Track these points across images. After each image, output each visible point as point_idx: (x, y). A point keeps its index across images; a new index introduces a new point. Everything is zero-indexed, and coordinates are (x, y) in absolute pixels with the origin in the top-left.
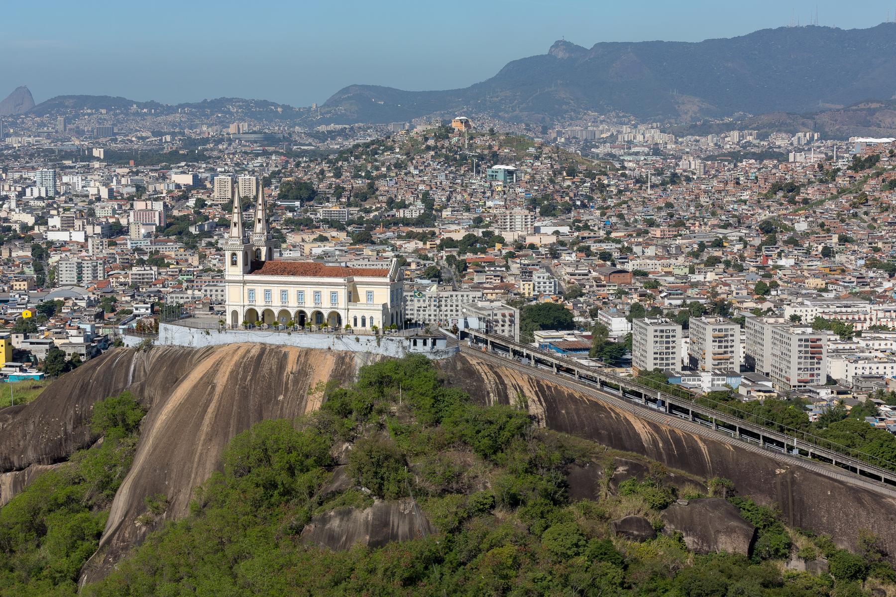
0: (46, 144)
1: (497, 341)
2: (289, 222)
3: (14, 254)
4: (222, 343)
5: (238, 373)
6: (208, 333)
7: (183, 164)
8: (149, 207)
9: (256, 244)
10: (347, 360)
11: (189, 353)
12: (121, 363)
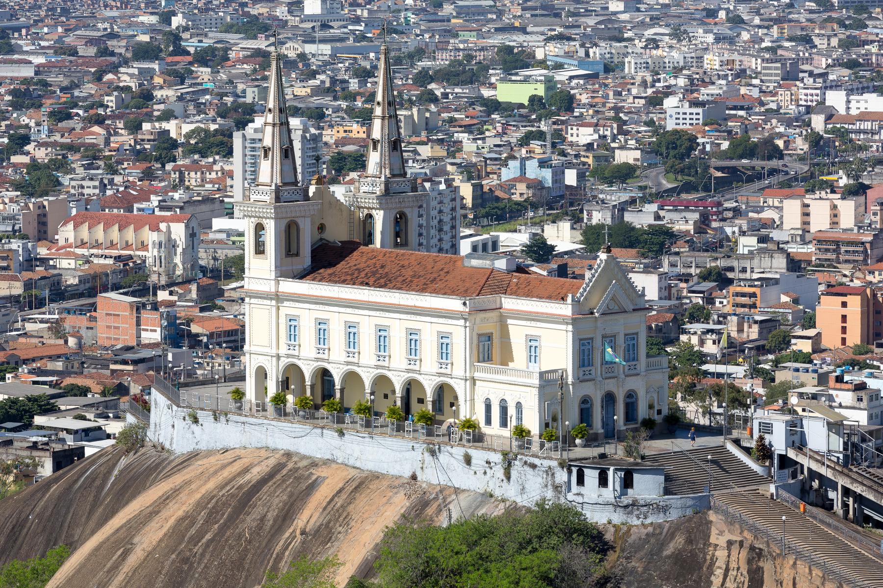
4: (219, 446)
5: (192, 524)
12: (92, 479)
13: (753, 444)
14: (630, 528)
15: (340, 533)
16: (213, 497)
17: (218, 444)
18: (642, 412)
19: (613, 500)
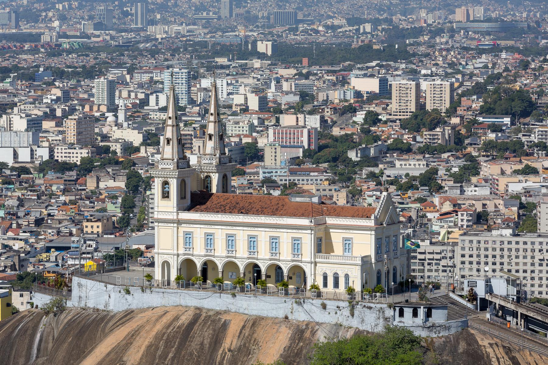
0: (201, 33)
1: (531, 314)
2: (489, 146)
3: (102, 185)
4: (145, 306)
5: (157, 348)
6: (128, 292)
7: (374, 64)
8: (301, 123)
9: (205, 169)
10: (307, 334)
11: (103, 319)
12: (24, 331)
13: (465, 293)
14: (432, 339)
15: (254, 349)
16: (164, 334)
17: (144, 305)
19: (422, 324)
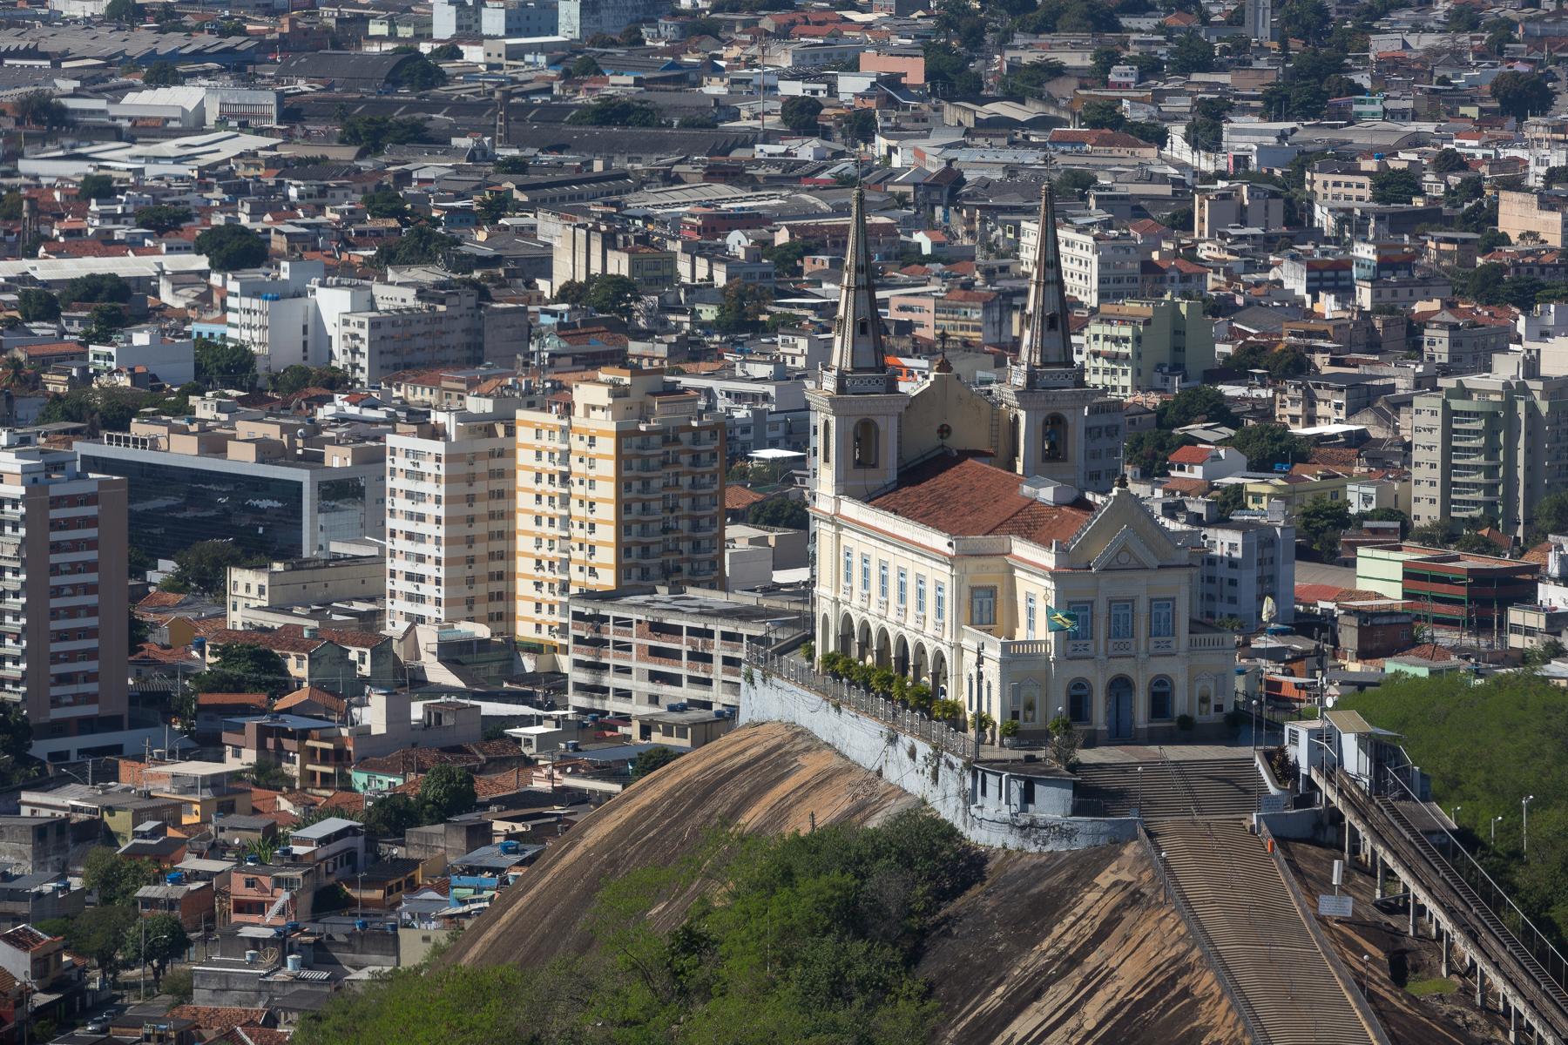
18: (1181, 703)
